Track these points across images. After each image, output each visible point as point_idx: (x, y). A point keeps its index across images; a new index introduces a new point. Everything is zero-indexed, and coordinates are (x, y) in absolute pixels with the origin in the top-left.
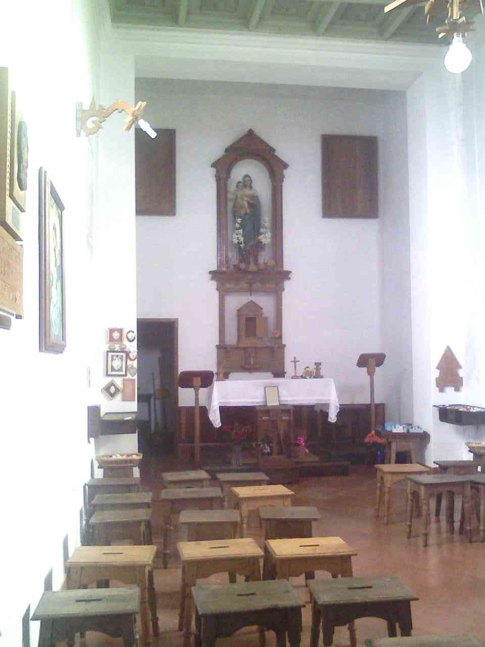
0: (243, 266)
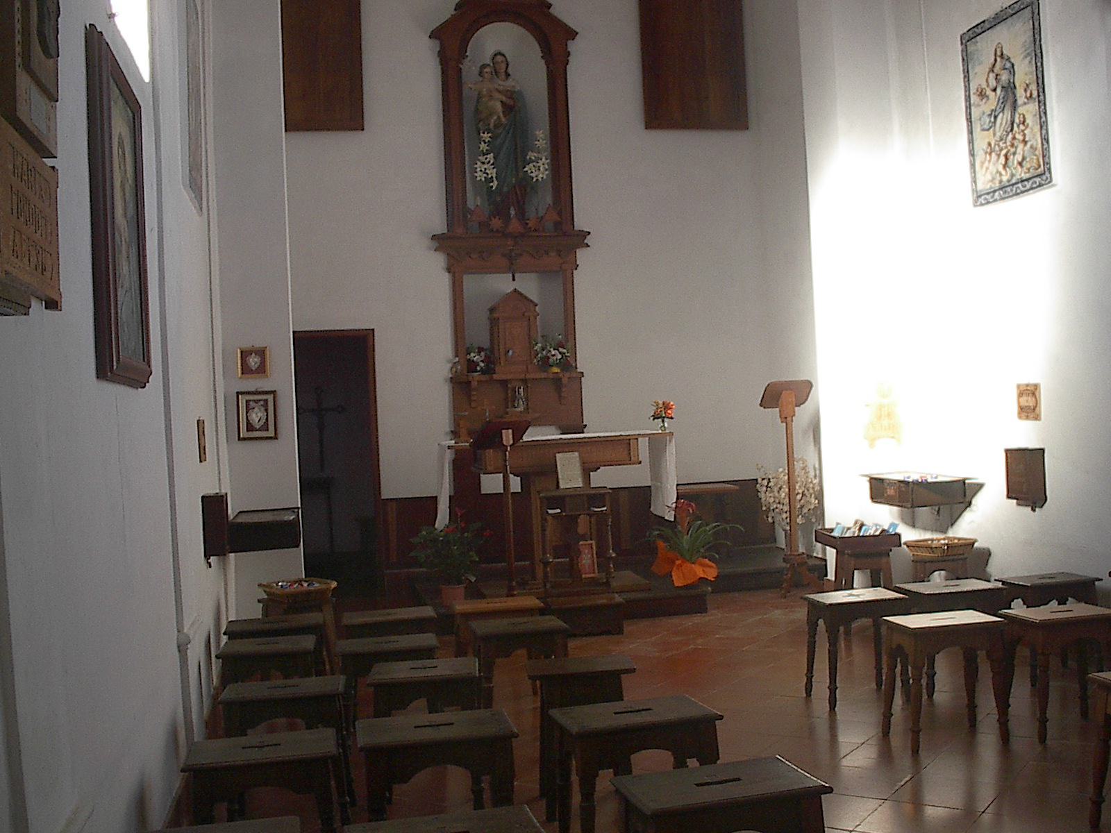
0: (496, 223)
